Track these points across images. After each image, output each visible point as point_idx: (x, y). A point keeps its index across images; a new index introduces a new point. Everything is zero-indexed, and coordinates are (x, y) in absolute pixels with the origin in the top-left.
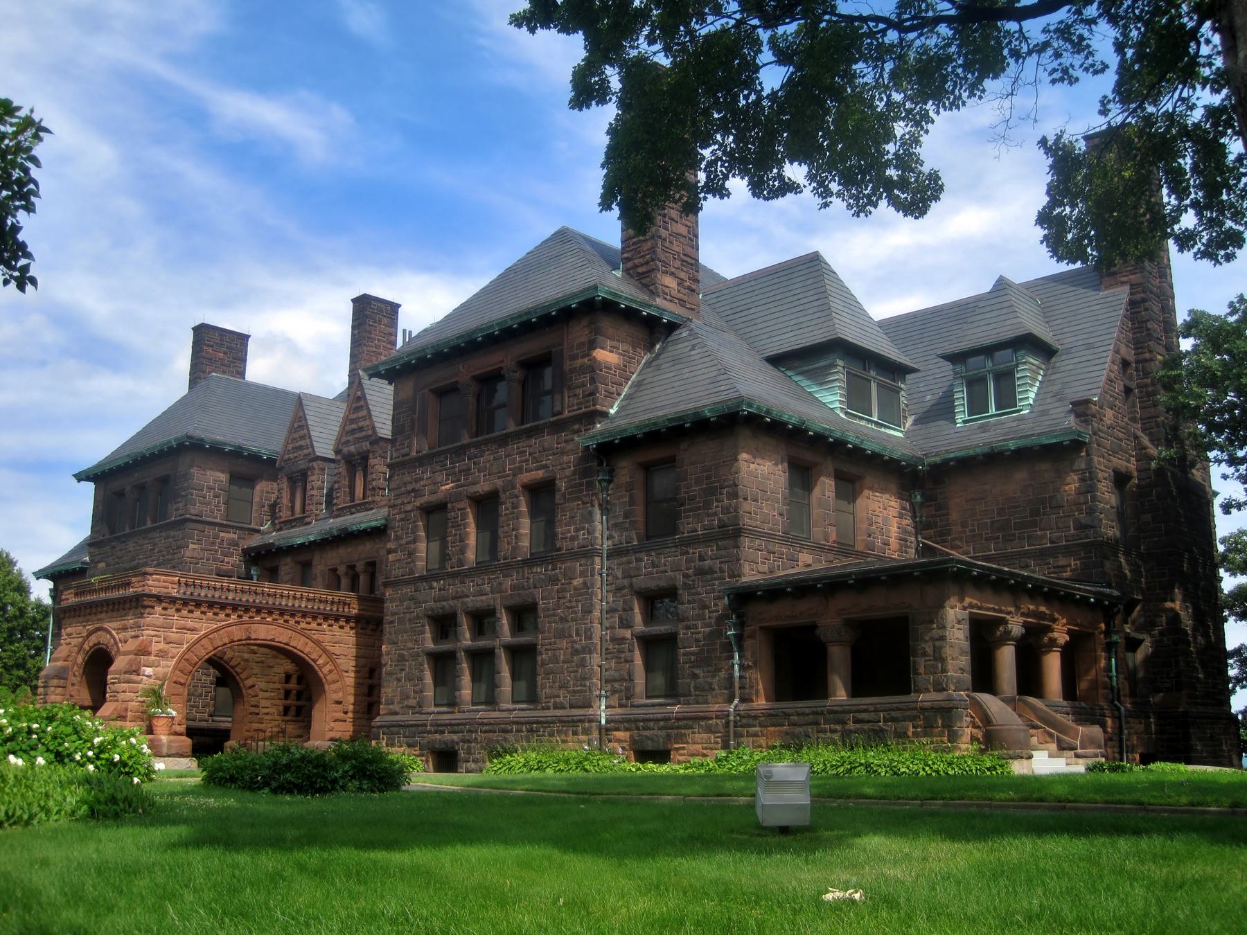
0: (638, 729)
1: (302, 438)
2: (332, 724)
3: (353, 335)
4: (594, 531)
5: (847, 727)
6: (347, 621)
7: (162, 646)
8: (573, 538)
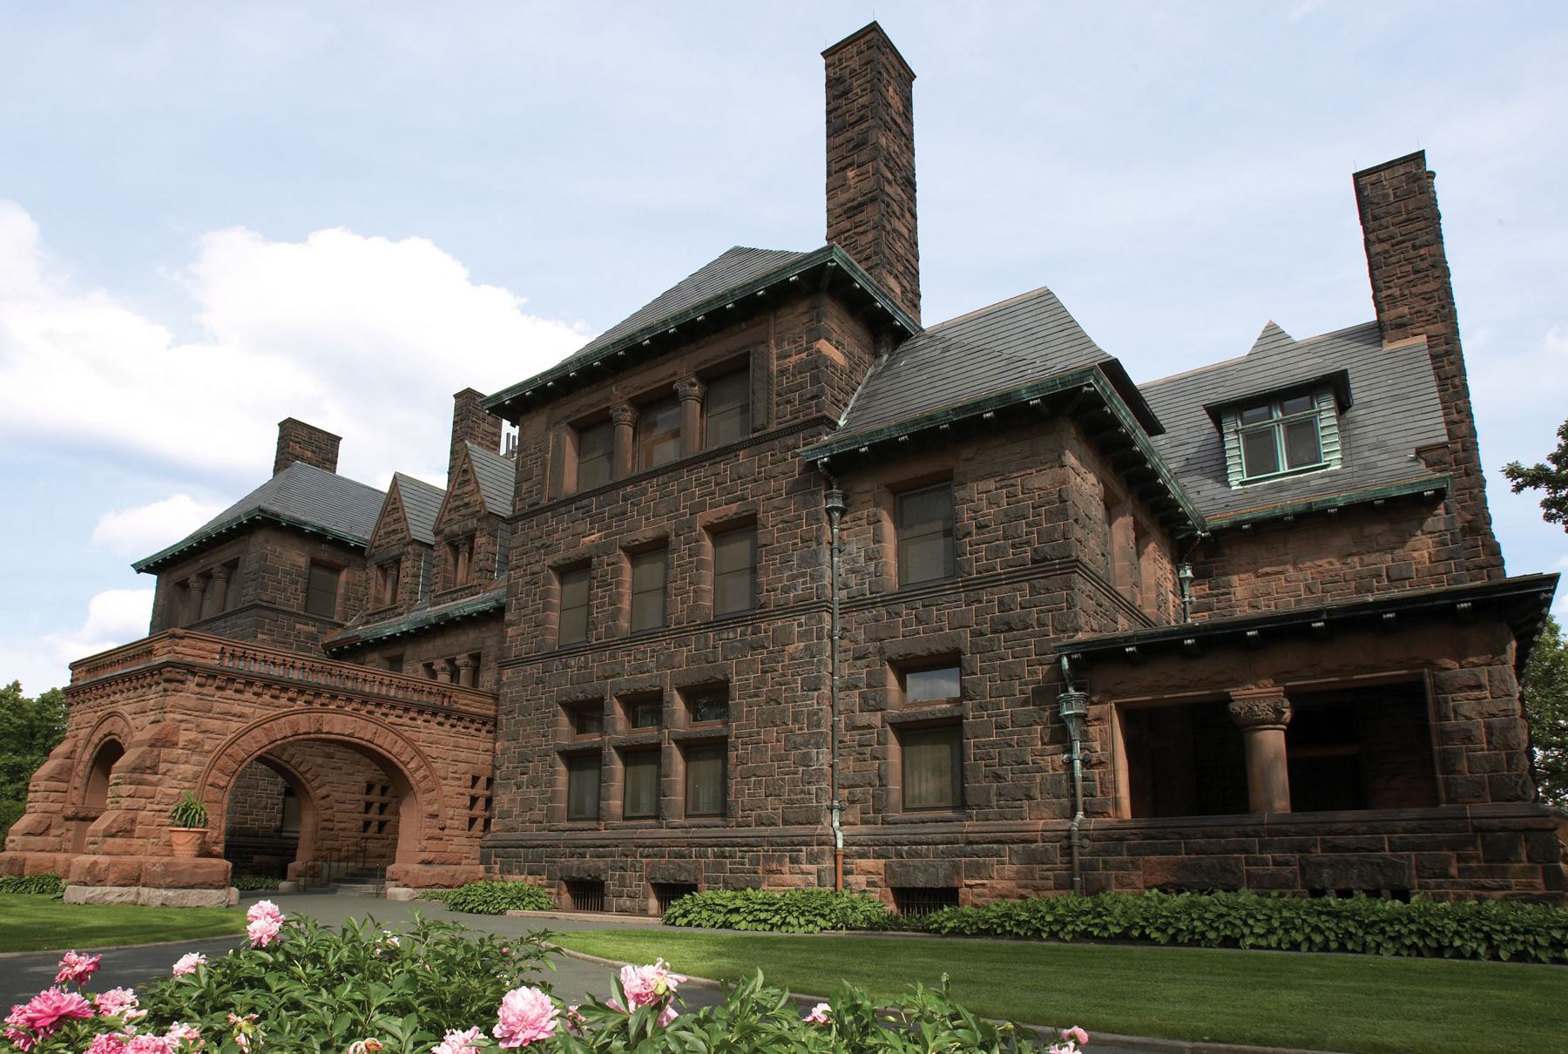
0: (899, 855)
1: (397, 520)
2: (424, 843)
3: (454, 431)
4: (822, 577)
5: (1311, 857)
6: (448, 717)
7: (192, 735)
8: (786, 590)
